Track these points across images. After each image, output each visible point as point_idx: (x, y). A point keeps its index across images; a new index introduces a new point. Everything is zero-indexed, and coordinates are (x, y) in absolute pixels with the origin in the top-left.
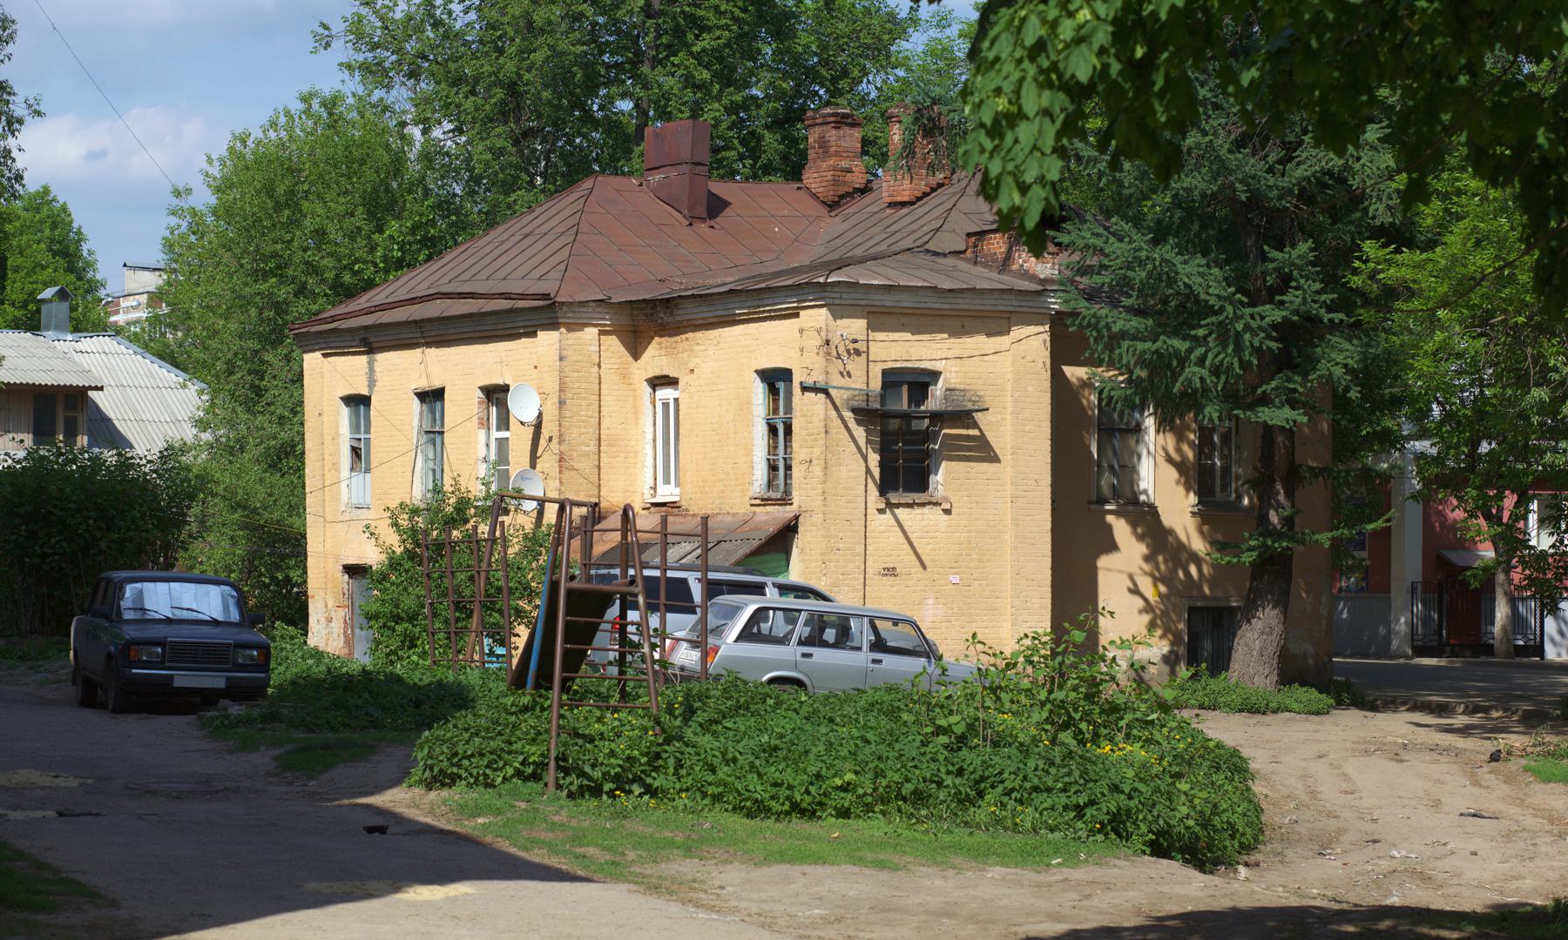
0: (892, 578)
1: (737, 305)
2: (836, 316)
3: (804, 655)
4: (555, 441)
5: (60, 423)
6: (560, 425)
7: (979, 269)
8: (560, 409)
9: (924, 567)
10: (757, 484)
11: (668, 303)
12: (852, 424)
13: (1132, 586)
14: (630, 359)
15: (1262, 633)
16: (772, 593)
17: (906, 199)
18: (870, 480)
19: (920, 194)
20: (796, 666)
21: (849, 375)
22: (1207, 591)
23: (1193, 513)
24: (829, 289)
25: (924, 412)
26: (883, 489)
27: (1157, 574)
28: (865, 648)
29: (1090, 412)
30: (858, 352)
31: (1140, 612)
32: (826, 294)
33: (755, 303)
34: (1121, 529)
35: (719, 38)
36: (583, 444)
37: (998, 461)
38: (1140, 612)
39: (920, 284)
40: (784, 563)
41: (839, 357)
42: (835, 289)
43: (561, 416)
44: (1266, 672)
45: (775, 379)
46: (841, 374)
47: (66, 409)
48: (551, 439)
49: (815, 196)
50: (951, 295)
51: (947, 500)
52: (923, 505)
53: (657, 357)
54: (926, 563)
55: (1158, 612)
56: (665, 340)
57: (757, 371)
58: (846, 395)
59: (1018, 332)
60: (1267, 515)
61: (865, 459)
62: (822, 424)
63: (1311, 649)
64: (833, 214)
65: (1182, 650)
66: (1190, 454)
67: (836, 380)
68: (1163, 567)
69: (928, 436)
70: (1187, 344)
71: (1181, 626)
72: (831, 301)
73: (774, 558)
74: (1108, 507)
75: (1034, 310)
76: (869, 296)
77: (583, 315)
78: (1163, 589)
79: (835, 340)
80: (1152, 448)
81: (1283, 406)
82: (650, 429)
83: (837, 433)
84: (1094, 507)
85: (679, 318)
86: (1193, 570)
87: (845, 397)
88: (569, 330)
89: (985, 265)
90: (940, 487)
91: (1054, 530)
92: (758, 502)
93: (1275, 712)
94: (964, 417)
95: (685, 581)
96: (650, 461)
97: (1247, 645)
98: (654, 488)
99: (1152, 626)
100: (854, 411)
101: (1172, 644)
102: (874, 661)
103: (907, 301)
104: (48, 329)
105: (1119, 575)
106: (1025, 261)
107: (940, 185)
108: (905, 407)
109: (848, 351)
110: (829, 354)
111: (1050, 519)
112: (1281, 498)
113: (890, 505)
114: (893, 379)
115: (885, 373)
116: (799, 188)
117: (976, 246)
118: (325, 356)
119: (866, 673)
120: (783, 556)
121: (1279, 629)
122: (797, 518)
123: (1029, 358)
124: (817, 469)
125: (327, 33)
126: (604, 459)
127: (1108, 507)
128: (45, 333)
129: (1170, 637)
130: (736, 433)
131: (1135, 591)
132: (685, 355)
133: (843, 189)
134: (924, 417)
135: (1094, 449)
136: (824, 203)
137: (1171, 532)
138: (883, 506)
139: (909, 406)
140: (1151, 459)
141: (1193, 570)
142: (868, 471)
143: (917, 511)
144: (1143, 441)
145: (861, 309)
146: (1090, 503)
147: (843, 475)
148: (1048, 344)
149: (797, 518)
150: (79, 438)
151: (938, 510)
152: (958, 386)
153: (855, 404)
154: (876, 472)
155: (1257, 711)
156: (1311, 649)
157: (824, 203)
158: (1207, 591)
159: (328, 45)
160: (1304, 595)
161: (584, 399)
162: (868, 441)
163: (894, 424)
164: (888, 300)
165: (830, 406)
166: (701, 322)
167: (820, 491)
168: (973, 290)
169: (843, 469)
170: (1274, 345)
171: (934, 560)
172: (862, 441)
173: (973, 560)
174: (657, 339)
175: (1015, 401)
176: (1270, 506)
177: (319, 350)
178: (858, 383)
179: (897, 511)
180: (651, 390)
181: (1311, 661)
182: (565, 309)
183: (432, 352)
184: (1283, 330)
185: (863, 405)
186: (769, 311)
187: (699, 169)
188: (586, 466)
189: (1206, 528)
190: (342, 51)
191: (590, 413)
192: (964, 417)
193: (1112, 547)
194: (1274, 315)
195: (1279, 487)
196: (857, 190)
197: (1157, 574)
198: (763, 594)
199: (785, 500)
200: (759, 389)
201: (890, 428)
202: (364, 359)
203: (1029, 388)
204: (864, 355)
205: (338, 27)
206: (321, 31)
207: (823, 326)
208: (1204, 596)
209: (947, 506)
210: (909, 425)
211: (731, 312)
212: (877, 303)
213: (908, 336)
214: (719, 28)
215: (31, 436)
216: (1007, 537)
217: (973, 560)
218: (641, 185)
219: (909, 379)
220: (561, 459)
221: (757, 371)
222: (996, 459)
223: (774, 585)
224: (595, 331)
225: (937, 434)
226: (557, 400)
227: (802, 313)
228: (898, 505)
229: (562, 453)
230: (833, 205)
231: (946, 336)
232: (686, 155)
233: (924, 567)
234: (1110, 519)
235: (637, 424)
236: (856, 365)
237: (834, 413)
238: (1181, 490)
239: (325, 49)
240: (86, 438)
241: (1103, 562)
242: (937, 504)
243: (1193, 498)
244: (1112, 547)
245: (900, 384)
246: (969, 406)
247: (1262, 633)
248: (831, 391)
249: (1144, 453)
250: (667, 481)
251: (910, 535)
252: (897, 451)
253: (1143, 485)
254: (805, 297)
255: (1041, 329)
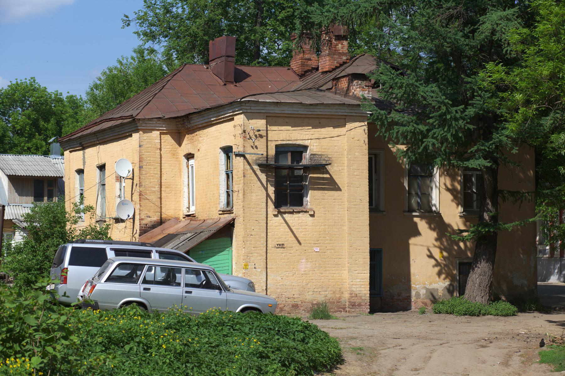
0: (282, 249)
1: (212, 116)
2: (249, 118)
3: (145, 289)
4: (138, 186)
5: (46, 192)
6: (140, 178)
7: (337, 96)
8: (140, 170)
9: (300, 244)
10: (222, 204)
11: (188, 117)
12: (258, 172)
13: (429, 253)
14: (177, 146)
15: (480, 275)
16: (155, 256)
17: (327, 70)
18: (269, 200)
19: (334, 67)
20: (140, 295)
21: (256, 147)
22: (469, 255)
23: (461, 217)
24: (244, 104)
25: (301, 166)
26: (278, 204)
27: (442, 247)
28: (182, 284)
29: (404, 167)
30: (261, 136)
31: (434, 266)
32: (242, 107)
33: (218, 114)
34: (422, 225)
35: (288, 12)
36: (152, 187)
37: (340, 190)
38: (434, 266)
39: (294, 102)
40: (230, 242)
41: (250, 138)
42: (247, 105)
43: (140, 174)
44: (482, 295)
45: (227, 150)
46: (252, 147)
47: (49, 186)
48: (137, 184)
49: (295, 72)
50: (312, 107)
51: (311, 210)
52: (299, 212)
53: (187, 146)
54: (301, 242)
55: (443, 265)
56: (190, 135)
57: (221, 148)
58: (255, 157)
59: (349, 126)
60: (483, 215)
61: (266, 189)
62: (242, 172)
63: (526, 282)
64: (301, 80)
65: (456, 284)
66: (459, 187)
67: (250, 150)
68: (445, 243)
69: (302, 178)
70: (427, 127)
71: (455, 272)
72: (245, 111)
73: (223, 241)
74: (414, 214)
75: (358, 114)
76: (266, 108)
77: (151, 125)
78: (445, 254)
79: (248, 130)
80: (438, 184)
81: (480, 158)
82: (186, 180)
83: (250, 177)
84: (406, 214)
85: (193, 125)
86: (462, 245)
87: (254, 158)
88: (144, 133)
89: (340, 94)
90: (309, 203)
91: (371, 225)
92: (221, 212)
93: (484, 315)
94: (321, 168)
95: (104, 250)
96: (186, 195)
97: (473, 281)
98: (189, 208)
99: (439, 274)
100: (260, 165)
101: (451, 281)
102: (187, 292)
103: (288, 110)
104: (52, 154)
105: (421, 247)
106: (355, 91)
107: (344, 63)
108: (289, 163)
109: (256, 136)
110: (245, 137)
111: (368, 219)
112: (490, 207)
113: (280, 212)
114: (281, 150)
115: (277, 147)
116: (288, 69)
117: (336, 85)
118: (71, 152)
119: (182, 299)
120: (229, 239)
121: (489, 273)
122: (234, 220)
123: (356, 139)
124: (241, 195)
125: (127, 19)
126: (163, 195)
127: (414, 214)
128: (50, 156)
129: (450, 278)
130: (214, 179)
131: (431, 256)
132: (196, 143)
133: (306, 68)
134: (300, 169)
135: (406, 185)
136: (298, 75)
137: (449, 226)
138: (276, 213)
139: (292, 162)
140: (438, 190)
141: (462, 245)
142: (268, 195)
143: (296, 215)
144: (433, 181)
145: (262, 114)
146: (404, 212)
147: (253, 198)
148: (367, 131)
149: (234, 220)
150: (54, 198)
151: (307, 215)
152: (317, 153)
153: (260, 162)
154: (273, 196)
155: (474, 315)
156: (526, 282)
157: (298, 75)
158: (469, 255)
159: (129, 25)
160: (522, 256)
161: (153, 165)
162: (267, 181)
163: (285, 172)
164: (277, 110)
165: (246, 163)
166: (200, 126)
167: (242, 206)
168: (323, 104)
169: (254, 194)
170: (471, 127)
171: (305, 240)
172: (264, 181)
173: (327, 240)
174: (187, 136)
175: (349, 160)
176: (484, 211)
177: (68, 149)
178: (262, 150)
179: (284, 216)
180: (186, 161)
181: (526, 289)
182: (141, 122)
183: (102, 147)
184: (476, 119)
185: (265, 162)
186: (223, 118)
187: (230, 59)
188: (154, 198)
189: (468, 223)
190: (135, 27)
191: (155, 172)
192: (321, 168)
193: (416, 233)
194: (471, 111)
195: (489, 201)
196: (313, 69)
197: (442, 247)
198: (150, 257)
199: (230, 212)
200: (223, 156)
201: (283, 174)
202: (81, 152)
203: (356, 154)
204: (265, 138)
205: (132, 16)
206: (125, 18)
207: (242, 123)
208: (468, 257)
209: (312, 213)
210: (293, 173)
211: (209, 120)
212: (271, 112)
213: (289, 128)
214: (289, 7)
215: (33, 197)
216: (345, 228)
217: (327, 240)
218: (207, 68)
219: (292, 149)
220: (140, 195)
221: (221, 148)
222: (339, 189)
223: (157, 251)
224: (158, 132)
225: (307, 177)
226: (138, 166)
227: (235, 118)
228: (285, 213)
229: (141, 191)
230: (302, 76)
231: (311, 128)
232: (224, 53)
233: (300, 244)
234: (416, 219)
235: (181, 177)
236: (261, 143)
237: (248, 167)
238: (454, 205)
239: (128, 26)
240: (57, 198)
241: (412, 241)
242: (306, 212)
243: (460, 209)
244: (416, 233)
245: (286, 152)
246: (324, 162)
247: (480, 275)
248: (246, 155)
249: (434, 187)
250: (193, 205)
251: (292, 228)
252: (286, 186)
253: (433, 202)
254: (234, 110)
255: (363, 124)
